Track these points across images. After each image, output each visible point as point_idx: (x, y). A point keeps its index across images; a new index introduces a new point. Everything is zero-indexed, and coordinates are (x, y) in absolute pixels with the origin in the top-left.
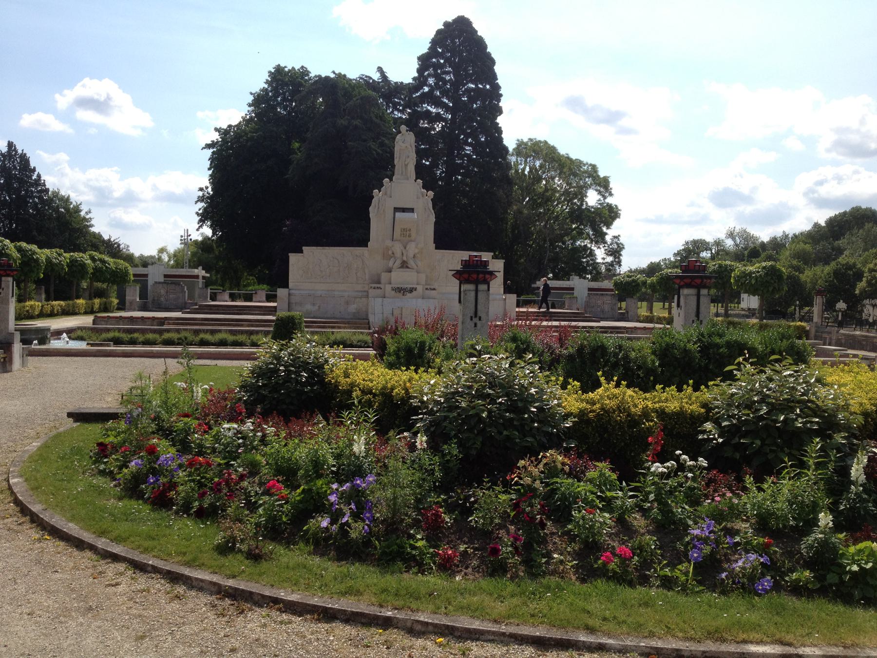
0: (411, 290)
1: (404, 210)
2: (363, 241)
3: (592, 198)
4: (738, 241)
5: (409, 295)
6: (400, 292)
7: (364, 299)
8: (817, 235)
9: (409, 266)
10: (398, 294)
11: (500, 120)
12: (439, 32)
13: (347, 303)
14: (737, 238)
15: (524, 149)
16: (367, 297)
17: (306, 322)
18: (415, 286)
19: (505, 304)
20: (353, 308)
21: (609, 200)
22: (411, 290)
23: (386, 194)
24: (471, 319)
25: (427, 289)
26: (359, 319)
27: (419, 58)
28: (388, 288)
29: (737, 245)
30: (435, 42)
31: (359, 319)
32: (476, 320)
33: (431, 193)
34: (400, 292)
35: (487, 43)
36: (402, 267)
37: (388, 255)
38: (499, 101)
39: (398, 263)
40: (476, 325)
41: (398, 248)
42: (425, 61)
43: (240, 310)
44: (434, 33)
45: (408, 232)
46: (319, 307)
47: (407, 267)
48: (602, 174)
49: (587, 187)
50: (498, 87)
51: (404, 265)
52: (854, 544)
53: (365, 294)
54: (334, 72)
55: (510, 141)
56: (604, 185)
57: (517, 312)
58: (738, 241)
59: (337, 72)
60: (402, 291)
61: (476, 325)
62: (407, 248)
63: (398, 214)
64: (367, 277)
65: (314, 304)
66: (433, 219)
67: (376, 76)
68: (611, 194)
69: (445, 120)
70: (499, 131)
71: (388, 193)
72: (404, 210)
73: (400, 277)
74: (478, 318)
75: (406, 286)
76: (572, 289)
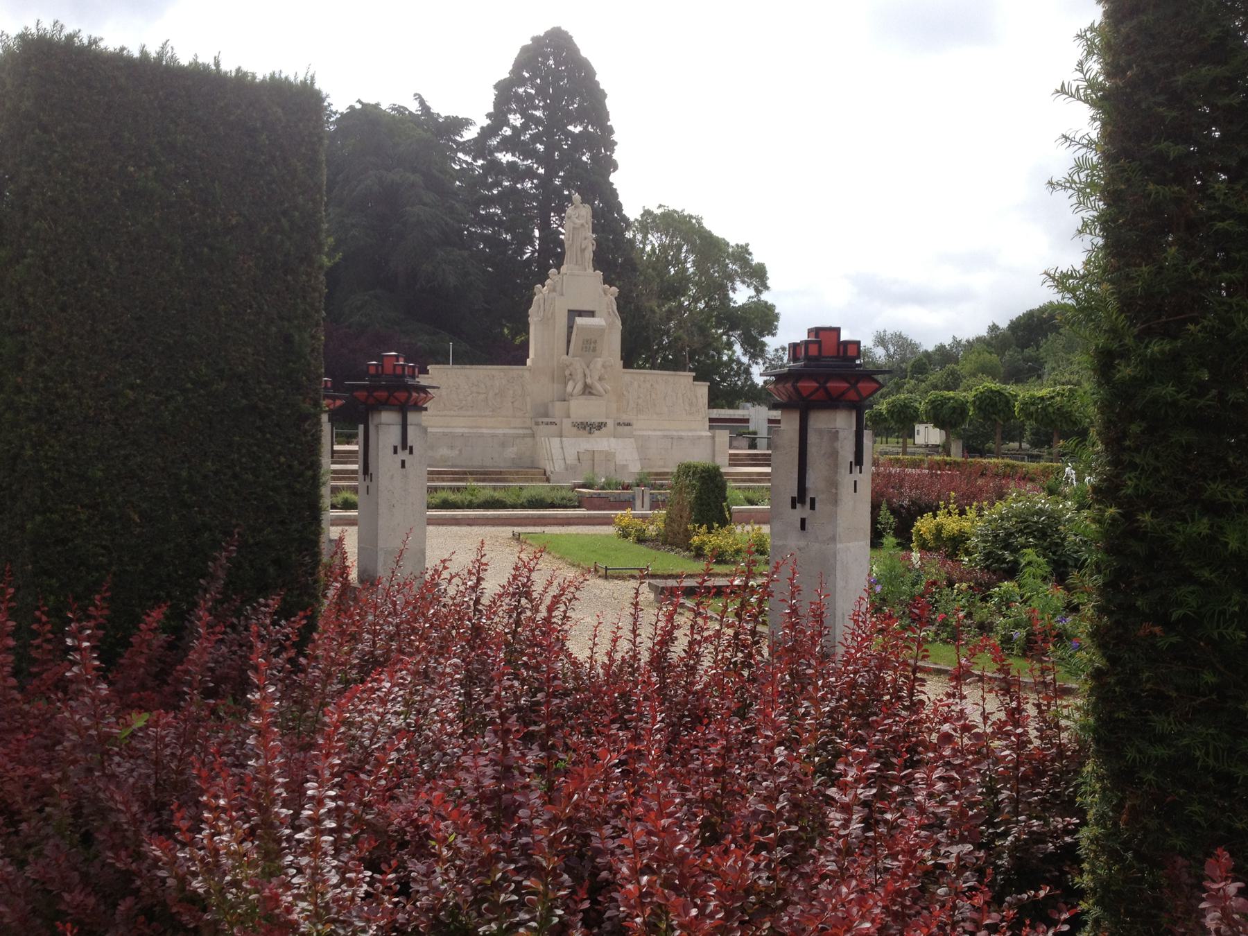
0: (600, 426)
1: (581, 313)
2: (518, 355)
3: (741, 295)
4: (892, 350)
5: (597, 432)
6: (585, 428)
7: (528, 440)
8: (997, 341)
9: (594, 392)
10: (582, 432)
11: (613, 178)
12: (525, 50)
13: (503, 445)
14: (890, 346)
15: (650, 221)
16: (533, 436)
17: (335, 472)
18: (604, 420)
19: (714, 442)
20: (511, 452)
21: (766, 297)
22: (600, 426)
23: (554, 290)
24: (395, 452)
25: (619, 424)
26: (522, 467)
27: (496, 87)
28: (567, 423)
29: (889, 355)
30: (519, 65)
31: (522, 467)
32: (403, 455)
33: (615, 290)
34: (585, 428)
35: (596, 69)
36: (583, 393)
37: (563, 377)
38: (613, 151)
39: (580, 386)
40: (403, 464)
41: (578, 365)
42: (505, 95)
43: (342, 457)
44: (518, 51)
45: (593, 345)
46: (460, 451)
47: (591, 393)
48: (756, 259)
49: (731, 277)
50: (610, 131)
51: (587, 390)
52: (1094, 739)
53: (528, 432)
54: (359, 101)
55: (632, 211)
56: (758, 276)
57: (730, 455)
58: (892, 350)
59: (365, 101)
60: (589, 427)
61: (403, 464)
62: (592, 366)
63: (579, 321)
64: (529, 407)
65: (452, 447)
66: (619, 323)
67: (414, 107)
68: (767, 288)
69: (538, 176)
70: (614, 194)
71: (558, 288)
72: (581, 313)
73: (582, 409)
74: (408, 451)
75: (593, 421)
76: (747, 421)
